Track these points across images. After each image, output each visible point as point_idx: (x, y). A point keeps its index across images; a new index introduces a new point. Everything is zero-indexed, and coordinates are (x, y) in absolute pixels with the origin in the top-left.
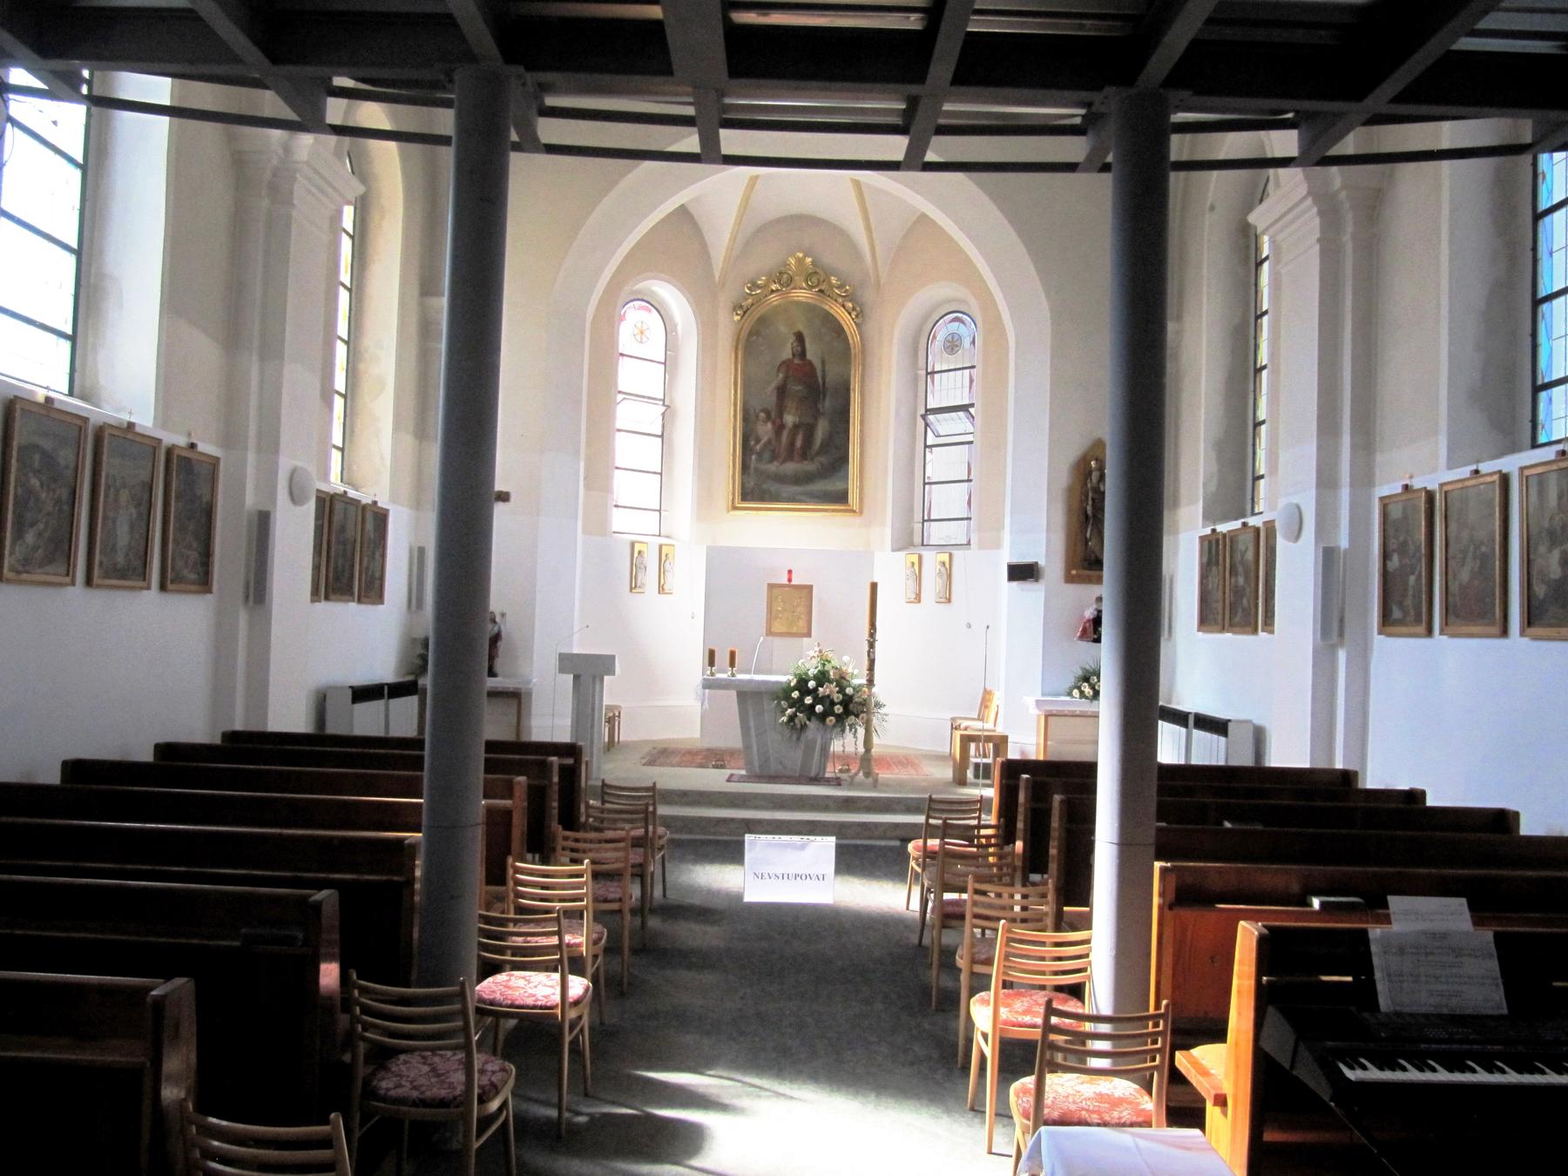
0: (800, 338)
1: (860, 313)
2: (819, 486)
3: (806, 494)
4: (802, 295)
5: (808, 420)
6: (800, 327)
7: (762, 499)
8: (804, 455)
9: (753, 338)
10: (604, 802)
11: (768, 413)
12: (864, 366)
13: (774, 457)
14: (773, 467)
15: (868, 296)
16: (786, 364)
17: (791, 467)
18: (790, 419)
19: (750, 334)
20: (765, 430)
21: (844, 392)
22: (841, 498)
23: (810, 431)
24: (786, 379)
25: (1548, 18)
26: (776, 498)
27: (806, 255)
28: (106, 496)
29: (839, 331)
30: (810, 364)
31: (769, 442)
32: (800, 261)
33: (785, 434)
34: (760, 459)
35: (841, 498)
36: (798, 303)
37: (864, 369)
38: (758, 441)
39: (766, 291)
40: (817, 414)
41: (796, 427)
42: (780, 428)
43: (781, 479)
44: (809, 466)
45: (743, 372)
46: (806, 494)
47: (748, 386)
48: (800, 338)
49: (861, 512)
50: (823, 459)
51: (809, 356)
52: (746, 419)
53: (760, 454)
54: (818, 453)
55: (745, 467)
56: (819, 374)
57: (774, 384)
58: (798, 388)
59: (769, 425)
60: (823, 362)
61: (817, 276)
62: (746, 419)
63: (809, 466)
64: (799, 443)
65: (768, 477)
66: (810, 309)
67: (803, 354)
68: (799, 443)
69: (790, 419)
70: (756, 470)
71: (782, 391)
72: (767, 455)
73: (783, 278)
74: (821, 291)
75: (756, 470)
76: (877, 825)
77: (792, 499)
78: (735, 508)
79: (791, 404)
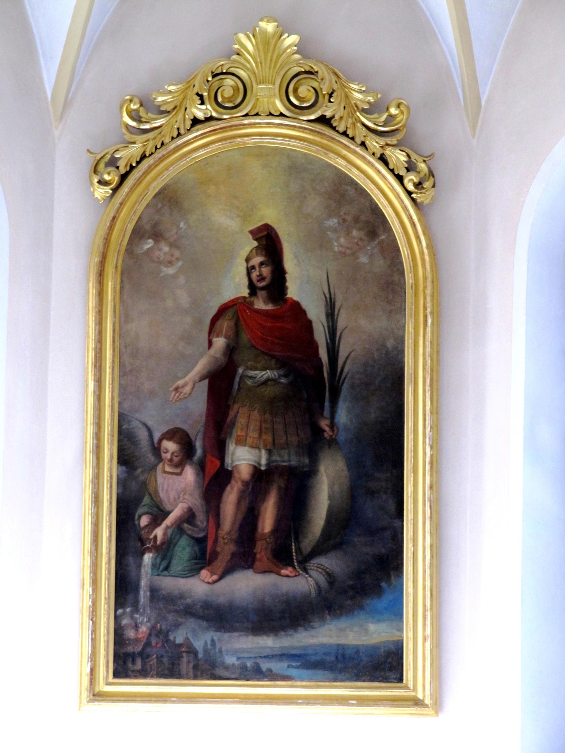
0: (268, 242)
1: (422, 179)
2: (327, 634)
3: (284, 656)
4: (278, 133)
5: (290, 458)
6: (270, 215)
7: (171, 672)
8: (285, 552)
9: (142, 247)
10: (355, 112)
11: (187, 448)
12: (438, 314)
13: (203, 558)
14: (198, 586)
15: (446, 133)
16: (232, 309)
17: (246, 585)
18: (243, 457)
19: (138, 234)
20: (178, 488)
21: (387, 382)
22: (385, 666)
23: (296, 489)
24: (231, 351)
25: (393, 215)
26: (207, 668)
27: (284, 29)
28: (401, 244)
29: (373, 223)
30: (297, 310)
31: (190, 517)
32: (268, 44)
33: (230, 499)
34: (164, 564)
35: (385, 666)
36: (261, 153)
37: (437, 324)
38: (159, 515)
39: (180, 121)
40: (315, 443)
41: (260, 478)
42: (216, 481)
43: (221, 617)
44: (297, 583)
45: (121, 334)
46: (284, 656)
47: (130, 368)
48: (268, 242)
49: (438, 705)
50: (332, 562)
51: (294, 291)
52: (126, 458)
53: (165, 551)
54: (319, 550)
55: (125, 587)
56: (320, 335)
57: (201, 366)
58: (259, 374)
59: (190, 474)
60: (331, 314)
61: (311, 92)
62: (129, 456)
63: (297, 583)
64: (267, 521)
65: (189, 612)
66: (296, 167)
67: (276, 285)
68: (267, 521)
69: (243, 457)
70: (154, 591)
71: (221, 383)
72: (183, 552)
73: (223, 92)
74: (323, 120)
75: (154, 591)
76: (254, 61)
77: (253, 672)
78: (97, 696)
79: (245, 418)
